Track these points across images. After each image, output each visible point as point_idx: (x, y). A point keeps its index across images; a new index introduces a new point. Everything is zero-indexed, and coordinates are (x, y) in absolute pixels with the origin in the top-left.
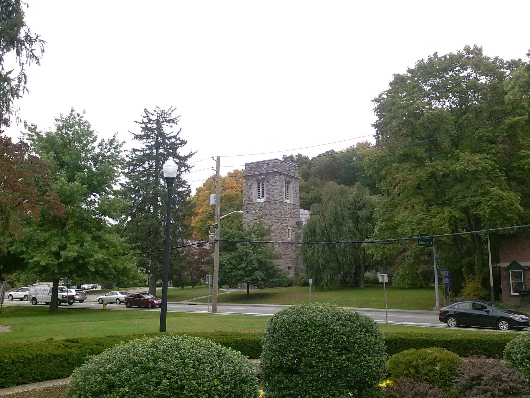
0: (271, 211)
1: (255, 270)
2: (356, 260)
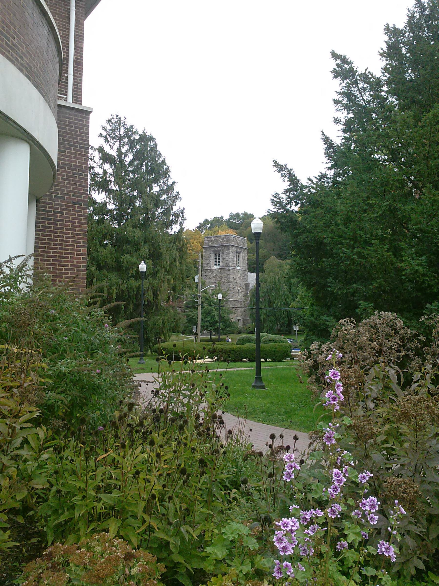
0: (226, 275)
1: (217, 322)
2: (289, 314)
